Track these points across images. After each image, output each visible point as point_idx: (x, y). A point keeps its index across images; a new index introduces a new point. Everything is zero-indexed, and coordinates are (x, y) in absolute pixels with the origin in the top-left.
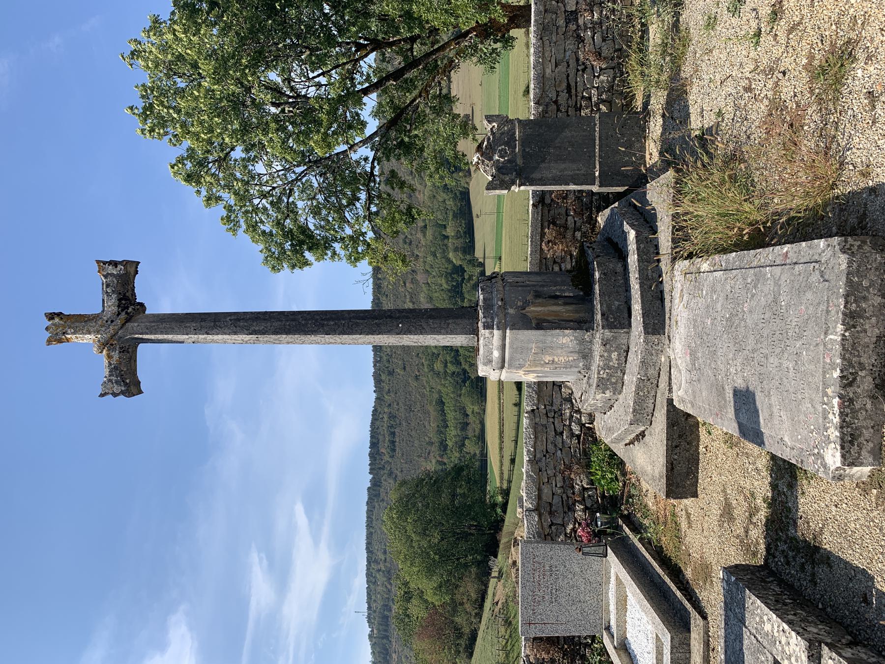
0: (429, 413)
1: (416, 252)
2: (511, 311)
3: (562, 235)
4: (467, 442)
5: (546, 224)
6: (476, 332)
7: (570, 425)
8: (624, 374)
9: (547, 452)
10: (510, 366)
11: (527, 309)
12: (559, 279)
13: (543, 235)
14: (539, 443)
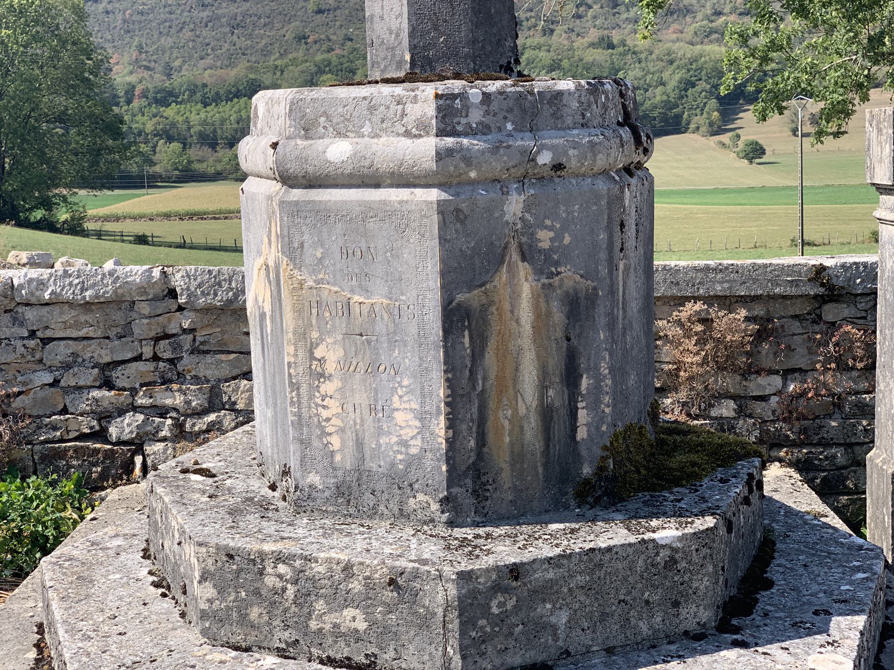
0: (231, 66)
1: (559, 29)
2: (514, 205)
3: (725, 360)
4: (176, 146)
5: (759, 310)
6: (421, 69)
7: (135, 409)
8: (282, 653)
9: (46, 341)
10: (293, 211)
11: (523, 269)
12: (632, 380)
13: (728, 302)
14: (69, 315)
